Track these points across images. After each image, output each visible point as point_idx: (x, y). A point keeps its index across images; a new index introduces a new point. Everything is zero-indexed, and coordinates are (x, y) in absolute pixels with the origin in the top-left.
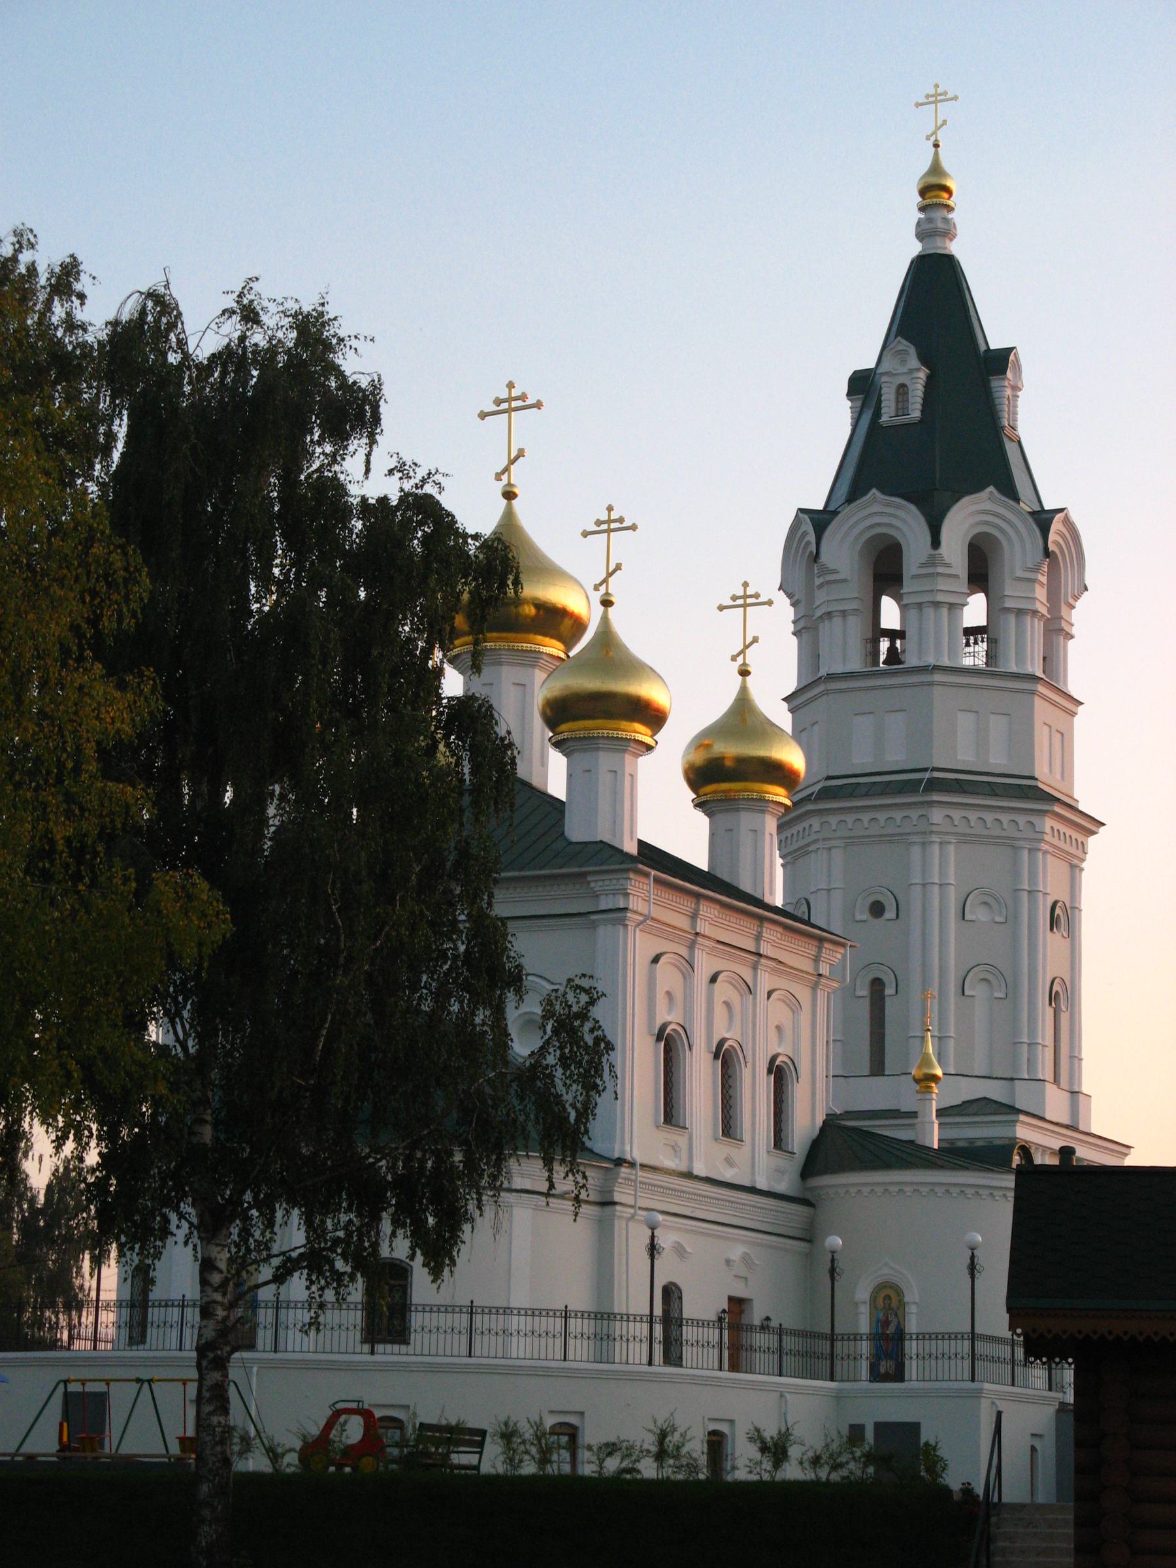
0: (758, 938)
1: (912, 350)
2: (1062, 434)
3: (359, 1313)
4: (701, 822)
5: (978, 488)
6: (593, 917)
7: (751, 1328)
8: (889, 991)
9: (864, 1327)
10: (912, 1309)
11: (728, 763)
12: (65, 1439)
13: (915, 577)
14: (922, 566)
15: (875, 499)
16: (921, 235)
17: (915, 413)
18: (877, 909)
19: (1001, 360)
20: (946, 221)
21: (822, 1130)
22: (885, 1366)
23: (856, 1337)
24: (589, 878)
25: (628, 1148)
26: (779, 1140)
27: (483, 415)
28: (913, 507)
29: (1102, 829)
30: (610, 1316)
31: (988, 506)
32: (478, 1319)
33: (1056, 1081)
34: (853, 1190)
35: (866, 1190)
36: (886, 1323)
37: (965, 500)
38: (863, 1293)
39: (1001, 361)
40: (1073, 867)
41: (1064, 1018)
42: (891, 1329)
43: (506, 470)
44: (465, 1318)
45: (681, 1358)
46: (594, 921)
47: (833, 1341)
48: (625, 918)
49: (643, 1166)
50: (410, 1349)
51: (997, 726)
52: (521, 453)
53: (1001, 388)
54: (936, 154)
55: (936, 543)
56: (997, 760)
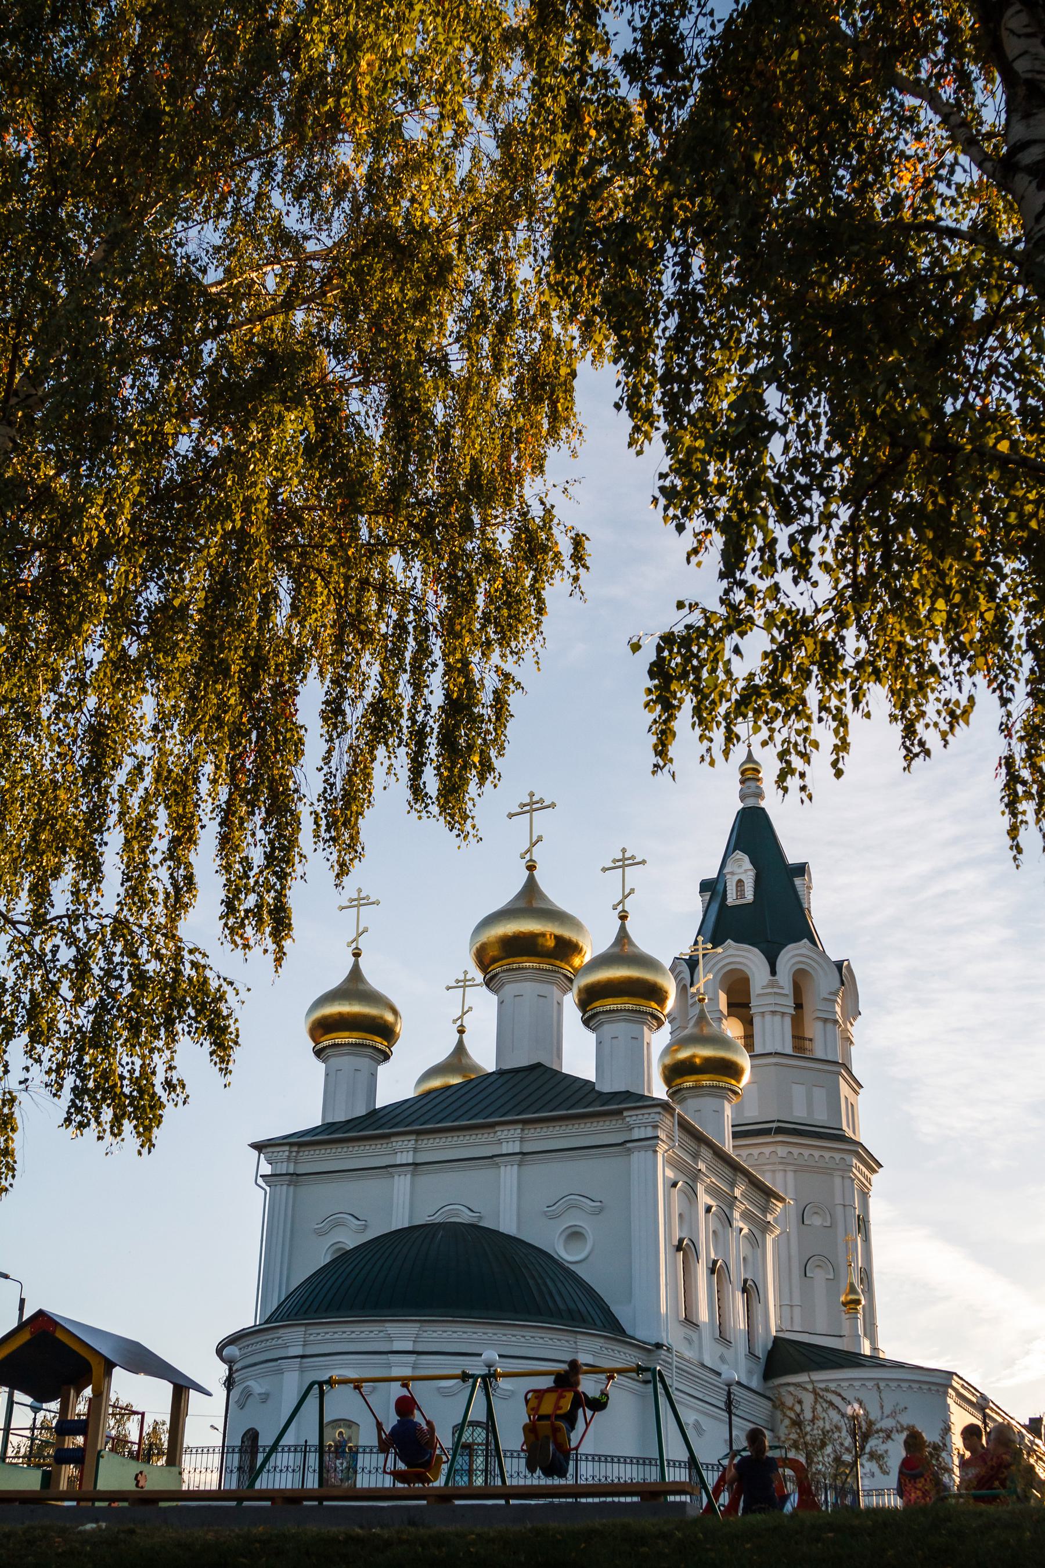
1: (746, 858)
6: (629, 1145)
11: (698, 1061)
12: (162, 1504)
13: (759, 995)
14: (764, 987)
15: (730, 946)
16: (742, 798)
17: (749, 896)
19: (801, 869)
20: (758, 787)
24: (625, 1114)
25: (664, 1335)
27: (511, 816)
28: (756, 950)
29: (880, 1170)
31: (804, 951)
43: (529, 851)
45: (754, 1512)
46: (629, 1149)
48: (657, 1145)
51: (820, 1095)
52: (540, 839)
54: (623, 928)
55: (773, 972)
56: (820, 1117)
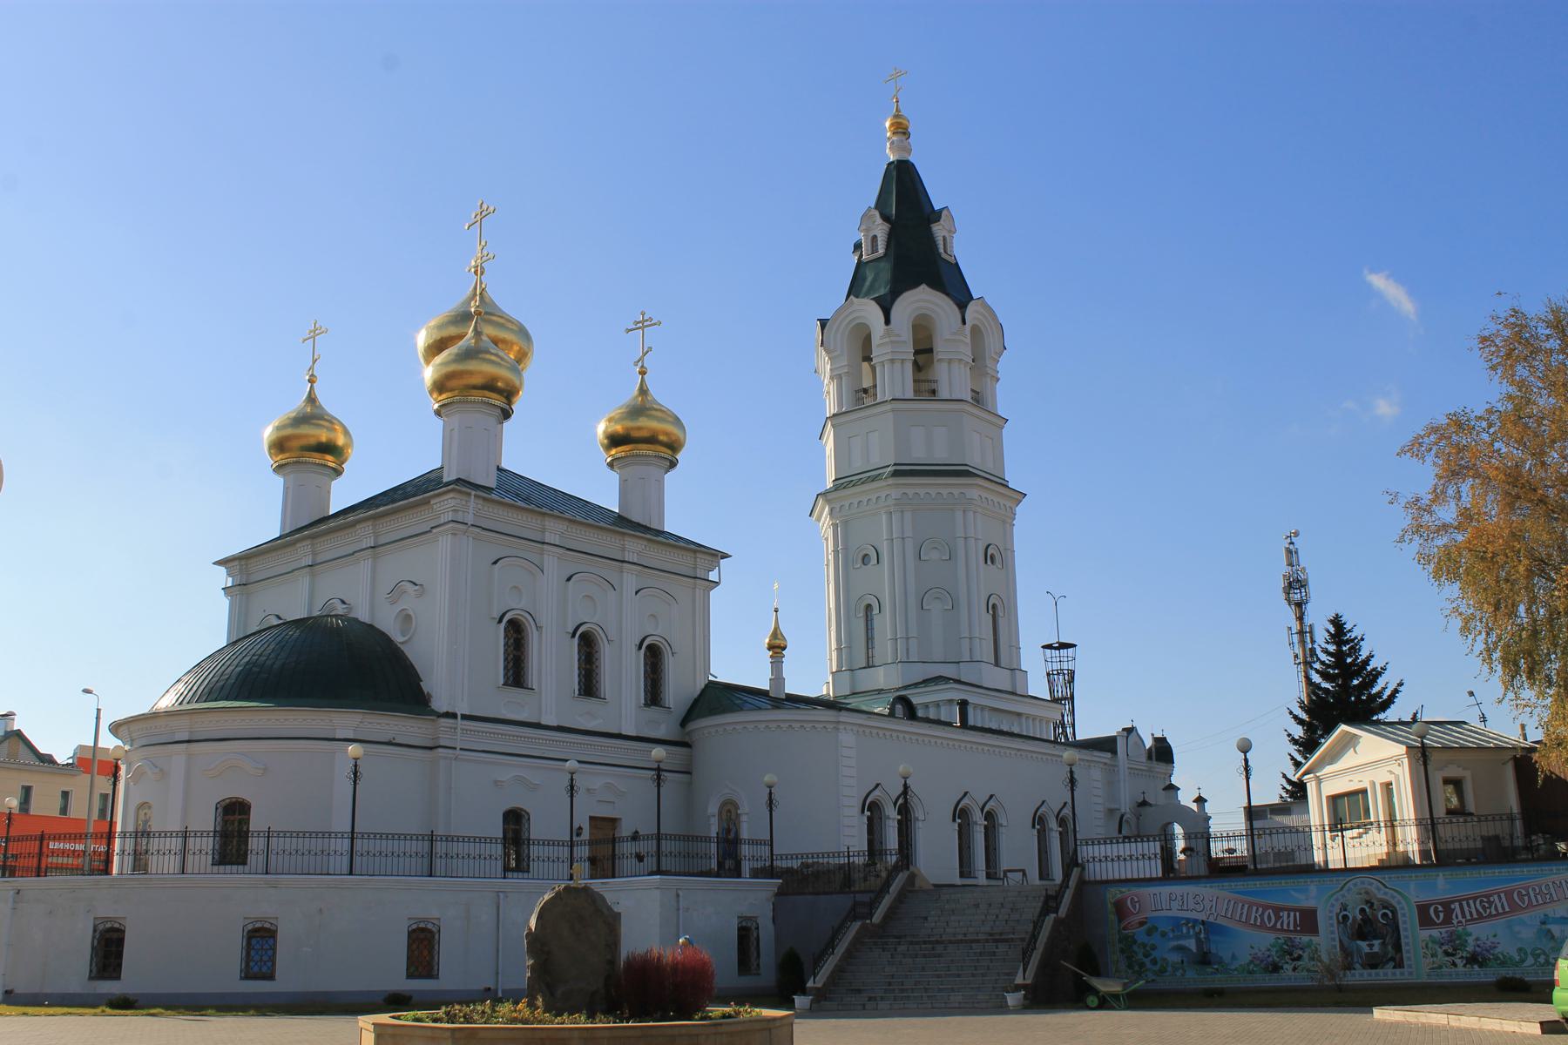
0: (543, 530)
2: (967, 244)
3: (1414, 829)
4: (614, 478)
5: (915, 285)
7: (622, 839)
8: (876, 611)
9: (714, 831)
10: (744, 818)
18: (865, 559)
21: (703, 691)
22: (729, 864)
23: (707, 839)
26: (654, 695)
30: (147, 834)
32: (273, 841)
33: (997, 664)
34: (729, 728)
35: (750, 727)
36: (729, 831)
37: (906, 295)
38: (713, 809)
39: (936, 216)
40: (1004, 522)
41: (1002, 622)
42: (732, 836)
44: (427, 844)
47: (659, 840)
49: (464, 717)
50: (247, 868)
53: (938, 230)
